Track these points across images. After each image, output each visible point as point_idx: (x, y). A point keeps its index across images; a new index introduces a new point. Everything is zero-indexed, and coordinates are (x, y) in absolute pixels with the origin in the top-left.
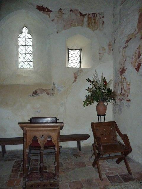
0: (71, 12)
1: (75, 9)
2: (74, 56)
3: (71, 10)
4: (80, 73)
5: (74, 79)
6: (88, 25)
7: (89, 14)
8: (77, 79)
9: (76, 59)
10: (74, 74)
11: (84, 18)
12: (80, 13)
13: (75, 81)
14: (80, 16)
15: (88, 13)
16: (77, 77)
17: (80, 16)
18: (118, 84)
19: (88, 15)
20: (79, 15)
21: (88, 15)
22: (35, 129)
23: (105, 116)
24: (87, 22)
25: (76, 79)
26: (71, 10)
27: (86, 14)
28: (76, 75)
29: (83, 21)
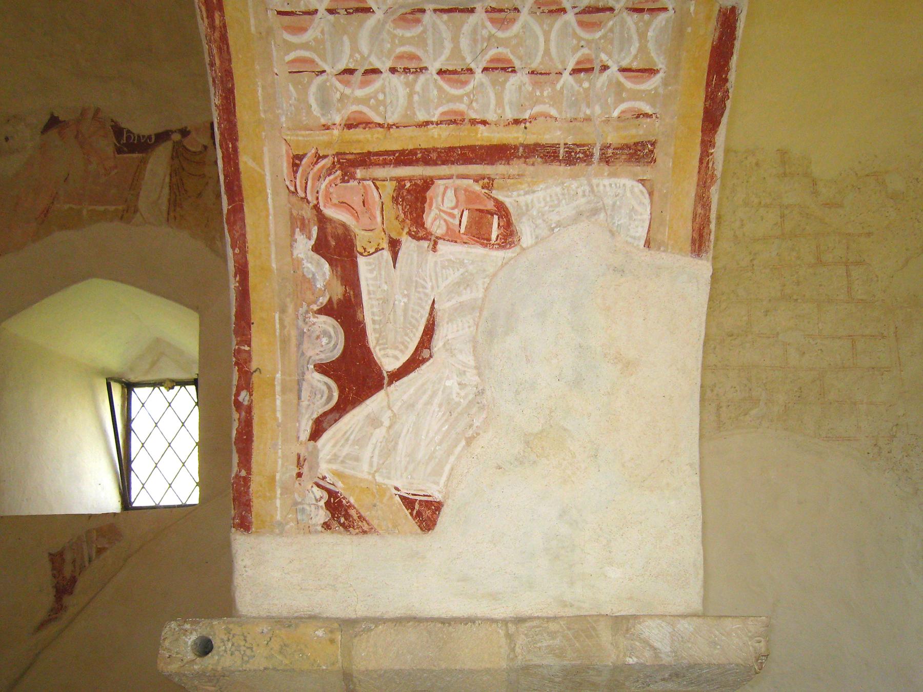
0: (53, 133)
1: (84, 113)
2: (170, 424)
3: (53, 122)
4: (100, 551)
5: (47, 599)
6: (174, 204)
7: (185, 133)
8: (73, 602)
9: (156, 445)
10: (57, 559)
11: (144, 162)
12: (118, 131)
13: (58, 608)
14: (119, 151)
15: (176, 125)
16: (74, 580)
17: (119, 151)
18: (306, 367)
19: (176, 137)
20: (106, 145)
21: (176, 137)
22: (349, 433)
23: (342, 408)
24: (166, 191)
25: (67, 600)
26: (53, 122)
27: (163, 136)
28: (68, 571)
29: (135, 184)
